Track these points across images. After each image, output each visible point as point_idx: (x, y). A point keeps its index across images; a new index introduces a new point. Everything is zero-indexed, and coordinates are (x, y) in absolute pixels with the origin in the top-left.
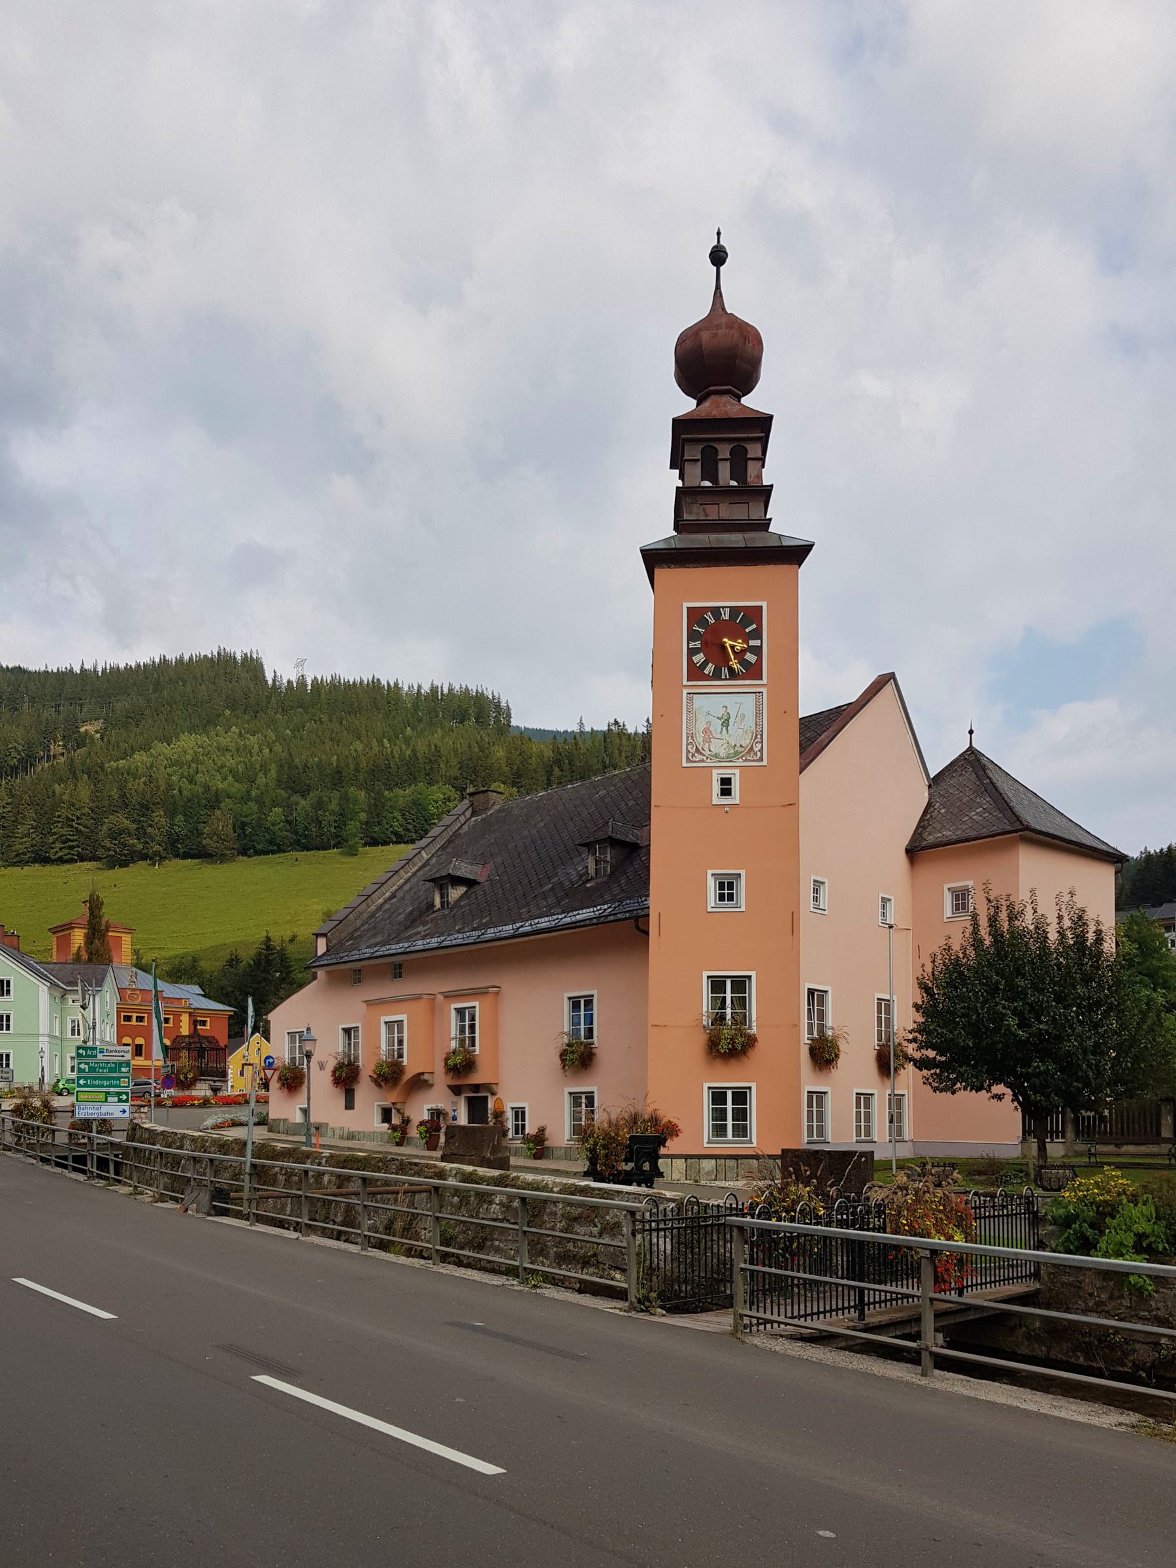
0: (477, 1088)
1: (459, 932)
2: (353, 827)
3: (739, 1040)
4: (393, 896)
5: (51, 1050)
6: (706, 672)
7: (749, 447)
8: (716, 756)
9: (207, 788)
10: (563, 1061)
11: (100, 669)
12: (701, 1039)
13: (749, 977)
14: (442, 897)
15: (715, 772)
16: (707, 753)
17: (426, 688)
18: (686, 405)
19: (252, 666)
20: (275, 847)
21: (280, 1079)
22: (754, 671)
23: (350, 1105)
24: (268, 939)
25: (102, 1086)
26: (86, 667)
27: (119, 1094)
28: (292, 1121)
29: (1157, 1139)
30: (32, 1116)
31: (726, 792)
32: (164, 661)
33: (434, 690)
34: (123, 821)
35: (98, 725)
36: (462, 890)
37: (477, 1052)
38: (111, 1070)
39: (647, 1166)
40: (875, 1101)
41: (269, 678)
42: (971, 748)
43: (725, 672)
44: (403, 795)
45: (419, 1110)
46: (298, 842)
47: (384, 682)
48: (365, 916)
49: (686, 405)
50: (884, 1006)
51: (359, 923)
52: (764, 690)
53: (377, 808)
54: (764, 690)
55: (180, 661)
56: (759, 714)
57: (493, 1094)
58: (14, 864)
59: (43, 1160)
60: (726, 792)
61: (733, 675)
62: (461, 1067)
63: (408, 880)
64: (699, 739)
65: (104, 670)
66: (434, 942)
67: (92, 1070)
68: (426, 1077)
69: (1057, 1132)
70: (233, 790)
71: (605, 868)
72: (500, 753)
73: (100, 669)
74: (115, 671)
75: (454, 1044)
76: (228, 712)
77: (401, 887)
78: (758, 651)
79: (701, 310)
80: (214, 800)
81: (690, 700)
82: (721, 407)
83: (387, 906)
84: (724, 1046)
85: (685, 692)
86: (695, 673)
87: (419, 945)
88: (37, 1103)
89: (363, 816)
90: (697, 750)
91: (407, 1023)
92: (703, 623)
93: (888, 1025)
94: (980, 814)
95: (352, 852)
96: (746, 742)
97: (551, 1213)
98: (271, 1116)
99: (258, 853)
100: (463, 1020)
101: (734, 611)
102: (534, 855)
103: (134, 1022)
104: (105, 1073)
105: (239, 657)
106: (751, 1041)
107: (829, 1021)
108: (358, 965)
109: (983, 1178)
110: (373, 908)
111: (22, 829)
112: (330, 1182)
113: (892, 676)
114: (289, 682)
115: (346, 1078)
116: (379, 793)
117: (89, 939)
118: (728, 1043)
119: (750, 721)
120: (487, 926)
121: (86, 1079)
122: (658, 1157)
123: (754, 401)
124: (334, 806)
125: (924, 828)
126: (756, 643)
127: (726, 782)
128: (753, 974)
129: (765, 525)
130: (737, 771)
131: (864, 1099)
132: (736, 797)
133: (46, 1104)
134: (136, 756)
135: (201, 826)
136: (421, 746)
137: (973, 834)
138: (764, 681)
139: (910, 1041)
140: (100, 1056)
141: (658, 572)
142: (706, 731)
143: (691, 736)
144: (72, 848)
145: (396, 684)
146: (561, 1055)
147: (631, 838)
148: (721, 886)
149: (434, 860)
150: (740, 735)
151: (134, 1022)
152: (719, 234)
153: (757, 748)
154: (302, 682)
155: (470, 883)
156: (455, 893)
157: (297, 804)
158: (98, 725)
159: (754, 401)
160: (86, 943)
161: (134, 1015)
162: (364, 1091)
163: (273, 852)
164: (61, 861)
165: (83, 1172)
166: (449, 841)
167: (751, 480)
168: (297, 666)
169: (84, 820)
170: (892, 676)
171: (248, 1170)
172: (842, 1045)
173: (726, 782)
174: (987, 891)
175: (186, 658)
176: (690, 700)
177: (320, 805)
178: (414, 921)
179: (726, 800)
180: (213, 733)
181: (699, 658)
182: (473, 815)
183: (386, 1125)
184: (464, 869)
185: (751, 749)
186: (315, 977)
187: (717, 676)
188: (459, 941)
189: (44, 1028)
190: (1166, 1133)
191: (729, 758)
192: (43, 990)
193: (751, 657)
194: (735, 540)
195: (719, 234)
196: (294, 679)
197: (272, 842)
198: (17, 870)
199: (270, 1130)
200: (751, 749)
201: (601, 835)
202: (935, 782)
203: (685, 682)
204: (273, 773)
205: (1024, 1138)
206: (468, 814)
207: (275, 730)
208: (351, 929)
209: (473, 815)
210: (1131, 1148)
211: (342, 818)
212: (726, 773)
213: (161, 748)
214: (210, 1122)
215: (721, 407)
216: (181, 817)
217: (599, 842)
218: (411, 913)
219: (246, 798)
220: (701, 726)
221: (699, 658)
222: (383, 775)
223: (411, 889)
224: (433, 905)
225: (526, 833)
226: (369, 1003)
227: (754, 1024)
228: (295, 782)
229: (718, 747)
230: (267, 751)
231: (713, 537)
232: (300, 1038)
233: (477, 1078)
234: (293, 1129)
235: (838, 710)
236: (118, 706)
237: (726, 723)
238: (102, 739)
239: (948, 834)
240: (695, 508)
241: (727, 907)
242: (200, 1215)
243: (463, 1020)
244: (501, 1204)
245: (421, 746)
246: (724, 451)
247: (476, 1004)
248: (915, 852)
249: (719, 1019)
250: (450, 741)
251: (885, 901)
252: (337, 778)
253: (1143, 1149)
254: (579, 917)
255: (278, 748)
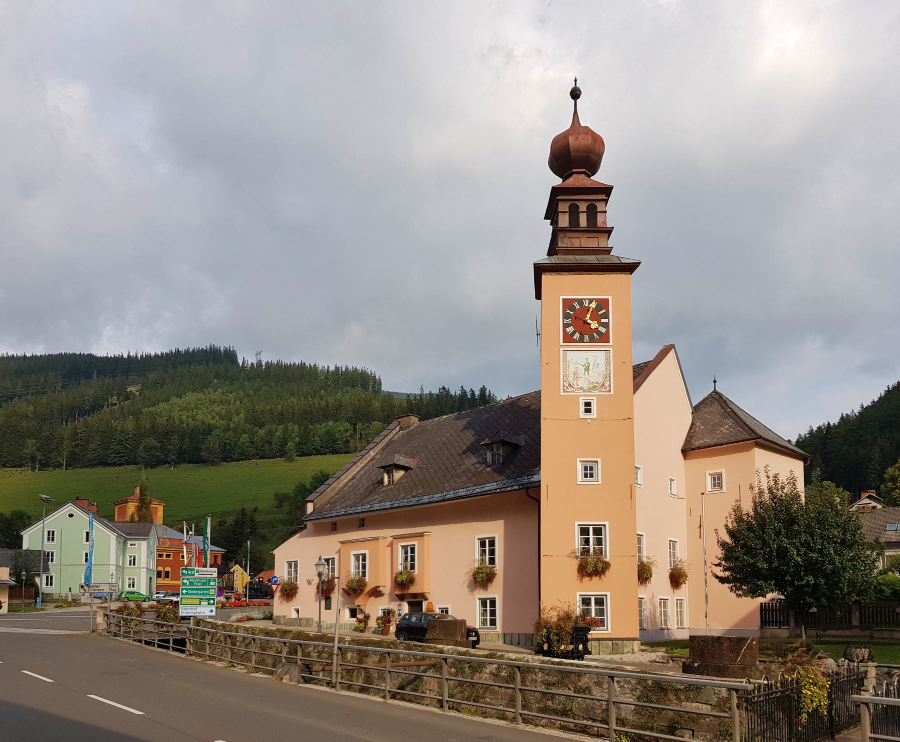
0: (415, 595)
1: (403, 498)
2: (291, 445)
3: (600, 565)
4: (354, 478)
5: (117, 574)
6: (575, 337)
7: (598, 204)
8: (581, 388)
9: (203, 423)
10: (475, 578)
11: (139, 356)
12: (574, 564)
13: (604, 525)
14: (389, 478)
15: (581, 398)
16: (576, 386)
17: (332, 368)
18: (557, 181)
19: (230, 356)
20: (244, 457)
21: (281, 590)
22: (605, 338)
23: (328, 607)
24: (243, 510)
25: (197, 594)
26: (131, 354)
27: (209, 599)
28: (288, 617)
29: (851, 627)
30: (129, 614)
31: (588, 411)
32: (178, 351)
33: (337, 369)
34: (152, 441)
35: (138, 387)
36: (401, 473)
37: (416, 573)
38: (203, 584)
39: (581, 647)
40: (669, 603)
41: (240, 362)
42: (715, 391)
43: (586, 337)
44: (321, 428)
45: (375, 608)
46: (258, 454)
47: (307, 364)
48: (337, 489)
49: (557, 181)
50: (673, 543)
51: (333, 494)
52: (611, 349)
53: (305, 435)
54: (611, 349)
55: (187, 352)
56: (608, 363)
57: (426, 599)
58: (86, 466)
59: (147, 643)
60: (588, 411)
61: (592, 340)
62: (403, 586)
63: (362, 468)
64: (571, 378)
65: (142, 357)
66: (387, 505)
67: (191, 583)
68: (381, 589)
69: (769, 622)
70: (219, 424)
71: (499, 460)
72: (377, 404)
73: (139, 356)
74: (148, 357)
75: (400, 568)
76: (215, 381)
77: (358, 472)
78: (606, 326)
79: (567, 125)
80: (209, 430)
81: (565, 355)
82: (577, 180)
83: (350, 484)
84: (590, 569)
85: (562, 349)
86: (568, 338)
87: (377, 506)
88: (132, 605)
89: (297, 439)
90: (570, 385)
91: (378, 553)
92: (573, 308)
93: (674, 557)
94: (727, 428)
95: (290, 459)
96: (600, 380)
97: (532, 680)
98: (275, 614)
99: (233, 460)
100: (406, 553)
101: (566, 316)
102: (446, 452)
103: (164, 558)
104: (200, 586)
105: (222, 349)
106: (607, 566)
107: (645, 553)
108: (335, 520)
109: (770, 652)
110: (342, 485)
111: (91, 446)
112: (352, 657)
113: (673, 346)
114: (252, 364)
115: (325, 591)
116: (306, 426)
117: (139, 509)
118: (592, 567)
119: (602, 368)
120: (423, 494)
121: (187, 589)
122: (587, 640)
123: (601, 177)
124: (279, 433)
125: (691, 437)
126: (605, 321)
127: (588, 404)
128: (607, 523)
129: (608, 251)
130: (595, 398)
131: (664, 601)
132: (594, 414)
133: (139, 606)
134: (161, 405)
135: (199, 445)
136: (331, 401)
137: (725, 441)
138: (611, 344)
139: (716, 565)
140: (196, 575)
141: (546, 278)
142: (575, 373)
143: (565, 376)
144: (121, 457)
145: (315, 365)
146: (474, 575)
147: (514, 441)
148: (586, 468)
149: (378, 456)
150: (596, 375)
151: (164, 558)
152: (576, 80)
153: (607, 384)
154: (259, 363)
155: (406, 469)
156: (398, 475)
157: (257, 432)
158: (138, 387)
159: (601, 177)
160: (137, 511)
161: (165, 554)
162: (337, 597)
163: (242, 460)
164: (114, 464)
165: (183, 652)
166: (387, 445)
167: (599, 224)
168: (257, 355)
169: (129, 441)
170: (673, 346)
171: (335, 652)
172: (654, 570)
173: (588, 404)
174: (766, 471)
175: (191, 350)
176: (565, 355)
177: (271, 433)
178: (370, 492)
179: (588, 416)
180: (206, 392)
181: (570, 329)
182: (401, 429)
183: (355, 619)
184: (403, 461)
185: (603, 385)
186: (305, 527)
187: (581, 340)
188: (404, 504)
189: (113, 561)
190: (855, 622)
191: (589, 390)
192: (113, 537)
193: (603, 330)
194: (591, 259)
195: (576, 80)
196: (255, 362)
197: (241, 454)
198: (88, 470)
199: (274, 623)
200: (603, 385)
201: (496, 439)
202: (696, 409)
203: (562, 344)
204: (242, 415)
205: (762, 626)
206: (397, 429)
207: (244, 391)
208: (328, 497)
209: (401, 429)
210: (833, 632)
211: (284, 443)
212: (588, 399)
213: (175, 400)
214: (234, 617)
215: (577, 180)
216: (187, 440)
217: (496, 443)
218: (367, 488)
219: (227, 429)
220: (572, 370)
221: (570, 329)
222: (308, 417)
223: (365, 473)
224: (382, 481)
225: (439, 439)
226: (342, 543)
227: (608, 554)
228: (256, 421)
229: (583, 383)
230: (238, 402)
231: (577, 257)
232: (293, 565)
233: (413, 590)
234: (292, 622)
235: (646, 364)
236: (150, 377)
237: (587, 369)
238: (140, 395)
239: (708, 441)
240: (566, 240)
241: (589, 482)
242: (293, 683)
243: (406, 553)
244: (491, 673)
245: (331, 401)
246: (583, 207)
247: (416, 543)
248: (687, 451)
249: (585, 552)
250: (349, 397)
251: (671, 480)
252: (282, 418)
253: (839, 632)
254: (486, 489)
255: (245, 400)
